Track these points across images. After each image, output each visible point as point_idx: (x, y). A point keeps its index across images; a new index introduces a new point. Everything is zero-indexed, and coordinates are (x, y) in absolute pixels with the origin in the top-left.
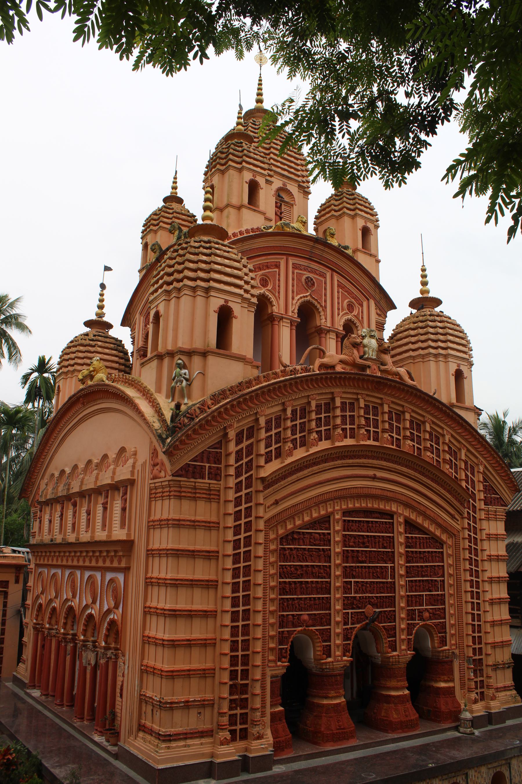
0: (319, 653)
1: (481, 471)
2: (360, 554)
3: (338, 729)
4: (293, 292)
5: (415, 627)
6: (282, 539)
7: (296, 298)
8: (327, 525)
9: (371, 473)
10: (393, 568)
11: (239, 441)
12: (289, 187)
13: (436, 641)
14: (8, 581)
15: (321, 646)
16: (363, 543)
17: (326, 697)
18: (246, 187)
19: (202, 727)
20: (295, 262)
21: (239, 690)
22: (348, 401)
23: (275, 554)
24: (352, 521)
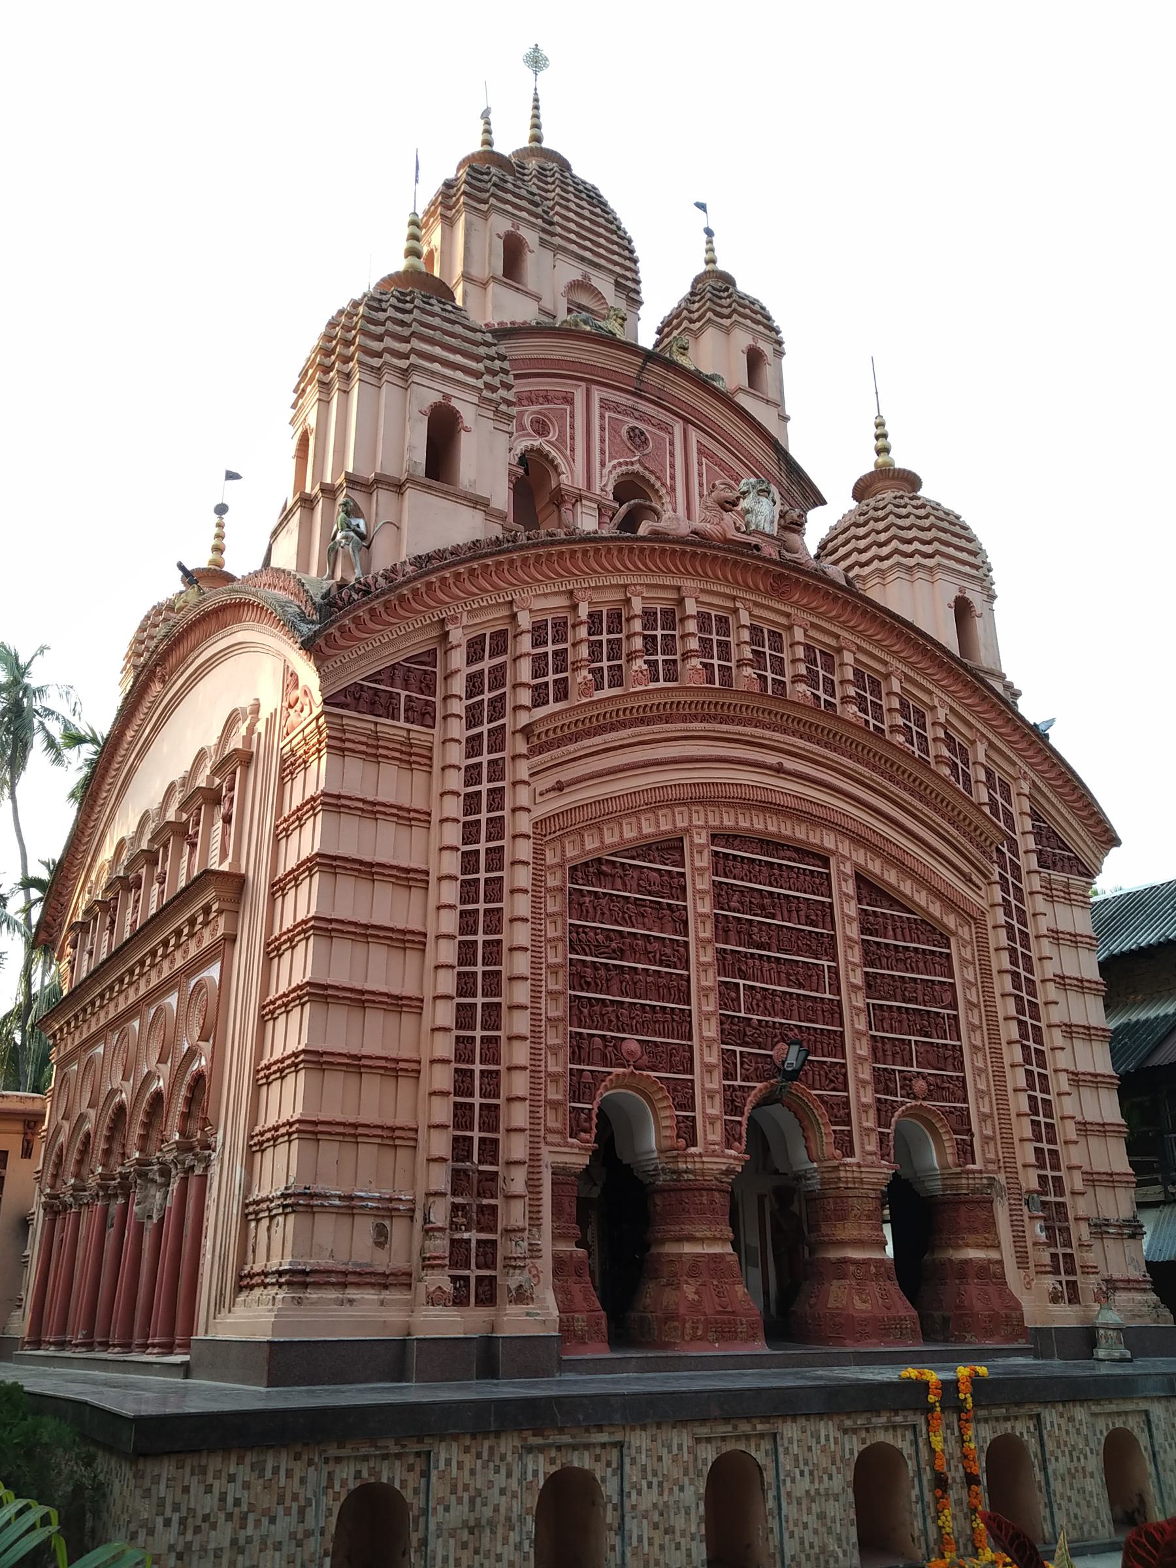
0: (668, 1133)
1: (1027, 791)
2: (755, 930)
3: (719, 1313)
4: (602, 452)
5: (894, 1109)
6: (574, 869)
7: (609, 465)
8: (677, 857)
9: (772, 759)
10: (834, 972)
11: (474, 655)
12: (595, 282)
13: (949, 1151)
14: (7, 1152)
15: (671, 1117)
16: (763, 907)
17: (691, 1239)
18: (499, 245)
19: (382, 1261)
20: (606, 396)
21: (475, 1178)
22: (713, 613)
23: (559, 898)
24: (735, 856)
